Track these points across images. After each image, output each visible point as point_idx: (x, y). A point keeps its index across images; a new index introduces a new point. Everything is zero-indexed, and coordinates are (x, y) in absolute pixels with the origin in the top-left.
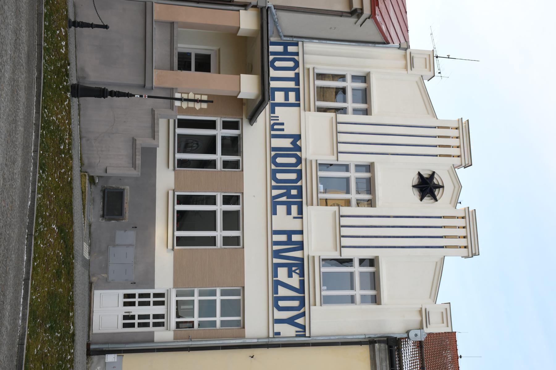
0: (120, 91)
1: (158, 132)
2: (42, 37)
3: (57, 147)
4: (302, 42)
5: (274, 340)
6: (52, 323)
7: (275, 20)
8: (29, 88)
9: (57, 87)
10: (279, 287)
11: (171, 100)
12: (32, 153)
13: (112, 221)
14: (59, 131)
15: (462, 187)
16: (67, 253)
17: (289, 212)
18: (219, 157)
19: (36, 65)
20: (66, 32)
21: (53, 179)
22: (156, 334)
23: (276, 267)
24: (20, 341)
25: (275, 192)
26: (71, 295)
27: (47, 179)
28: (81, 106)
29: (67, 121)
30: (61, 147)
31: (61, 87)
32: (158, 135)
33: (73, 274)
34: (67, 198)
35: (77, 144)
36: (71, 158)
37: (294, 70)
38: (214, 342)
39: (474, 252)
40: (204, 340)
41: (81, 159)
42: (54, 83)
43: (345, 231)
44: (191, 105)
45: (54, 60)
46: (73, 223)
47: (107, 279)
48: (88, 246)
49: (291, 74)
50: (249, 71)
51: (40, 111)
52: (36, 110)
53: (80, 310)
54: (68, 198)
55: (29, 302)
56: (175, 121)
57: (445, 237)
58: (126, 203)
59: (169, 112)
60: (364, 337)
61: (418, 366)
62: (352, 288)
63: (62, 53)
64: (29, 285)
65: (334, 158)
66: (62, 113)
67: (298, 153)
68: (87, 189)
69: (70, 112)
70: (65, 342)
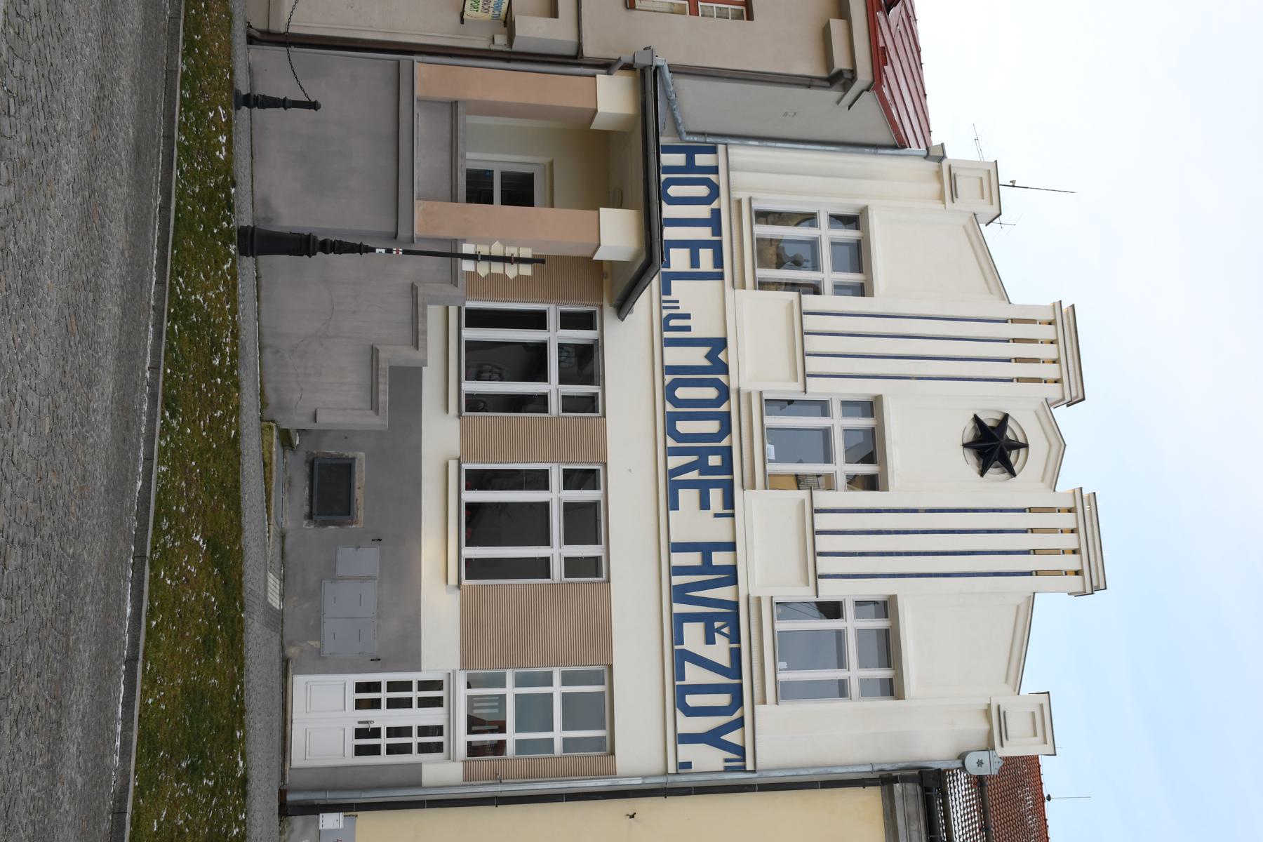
0: (344, 240)
1: (425, 332)
2: (174, 122)
3: (206, 362)
4: (724, 146)
5: (678, 778)
6: (195, 757)
7: (670, 96)
8: (138, 223)
9: (208, 229)
10: (688, 665)
11: (453, 259)
12: (146, 372)
13: (330, 527)
14: (209, 327)
15: (1065, 445)
16: (228, 598)
17: (705, 505)
18: (553, 388)
19: (160, 179)
20: (229, 120)
21: (196, 431)
22: (424, 768)
23: (679, 621)
24: (117, 804)
25: (675, 462)
26: (238, 692)
27: (182, 432)
28: (263, 281)
29: (229, 306)
30: (214, 362)
31: (215, 231)
32: (426, 340)
33: (243, 644)
34: (228, 475)
35: (252, 360)
36: (237, 386)
37: (710, 204)
38: (549, 786)
39: (1095, 583)
40: (528, 780)
41: (262, 393)
42: (201, 221)
43: (824, 543)
44: (497, 268)
45: (202, 173)
46: (240, 530)
47: (319, 651)
48: (278, 582)
49: (703, 212)
50: (618, 202)
51: (165, 278)
52: (158, 276)
53: (260, 722)
54: (230, 475)
55: (136, 713)
56: (459, 309)
57: (1035, 552)
58: (359, 488)
59: (449, 290)
60: (869, 769)
61: (977, 825)
62: (841, 663)
63: (220, 159)
64: (136, 673)
65: (798, 386)
66: (218, 288)
67: (722, 378)
68: (275, 458)
69: (235, 286)
70: (225, 797)
